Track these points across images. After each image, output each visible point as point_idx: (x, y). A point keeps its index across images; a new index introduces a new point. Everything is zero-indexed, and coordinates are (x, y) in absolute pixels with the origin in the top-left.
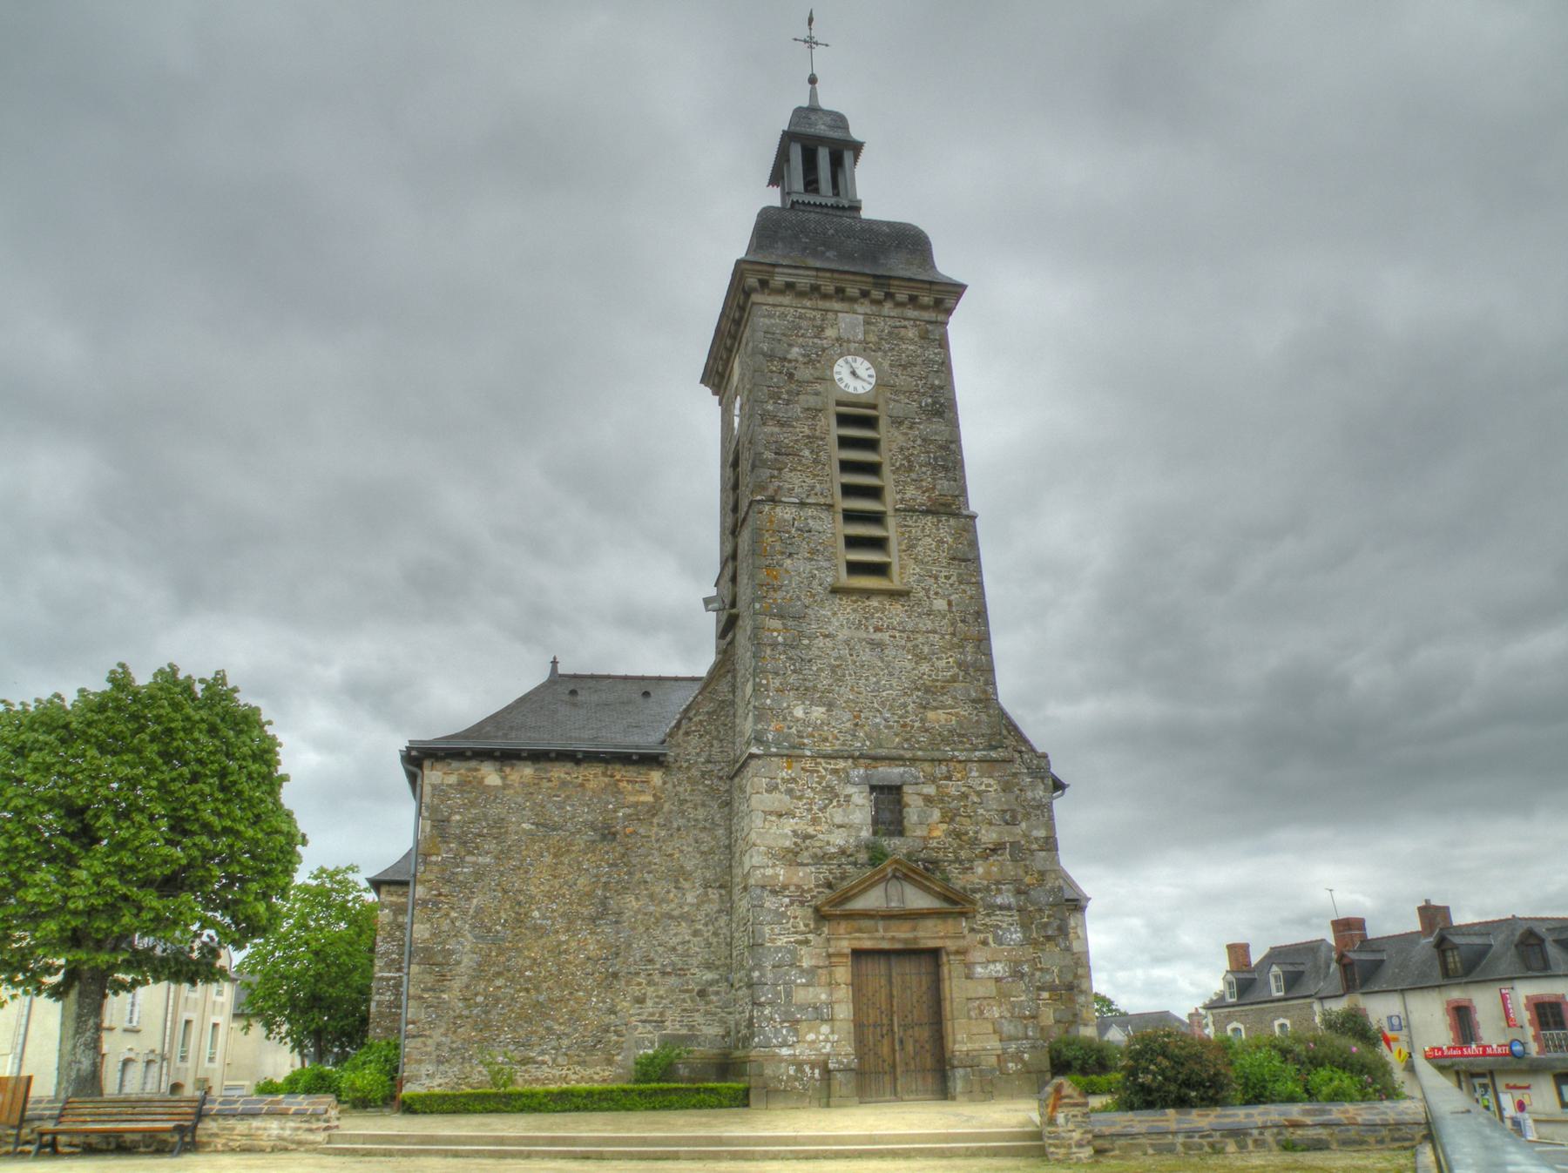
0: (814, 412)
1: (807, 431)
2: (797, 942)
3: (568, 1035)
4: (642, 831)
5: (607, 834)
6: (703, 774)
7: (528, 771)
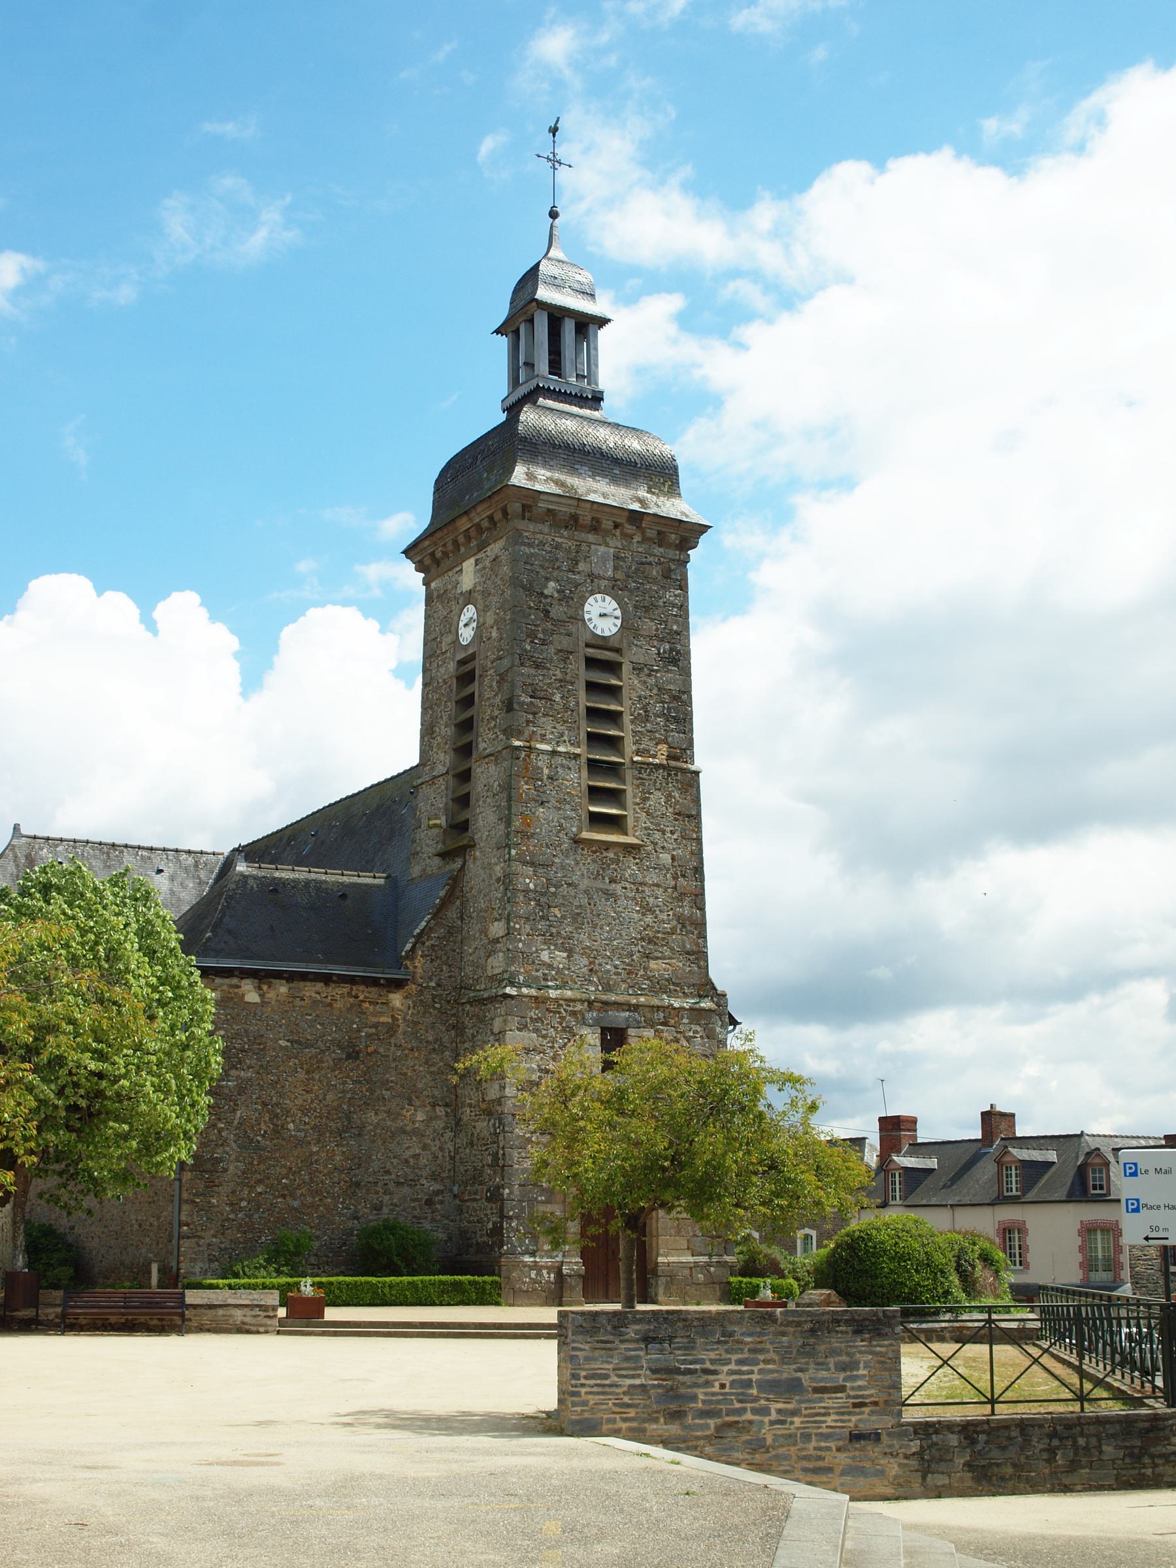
0: (565, 654)
1: (559, 676)
3: (318, 1238)
4: (381, 1050)
5: (353, 1054)
6: (434, 997)
7: (283, 989)
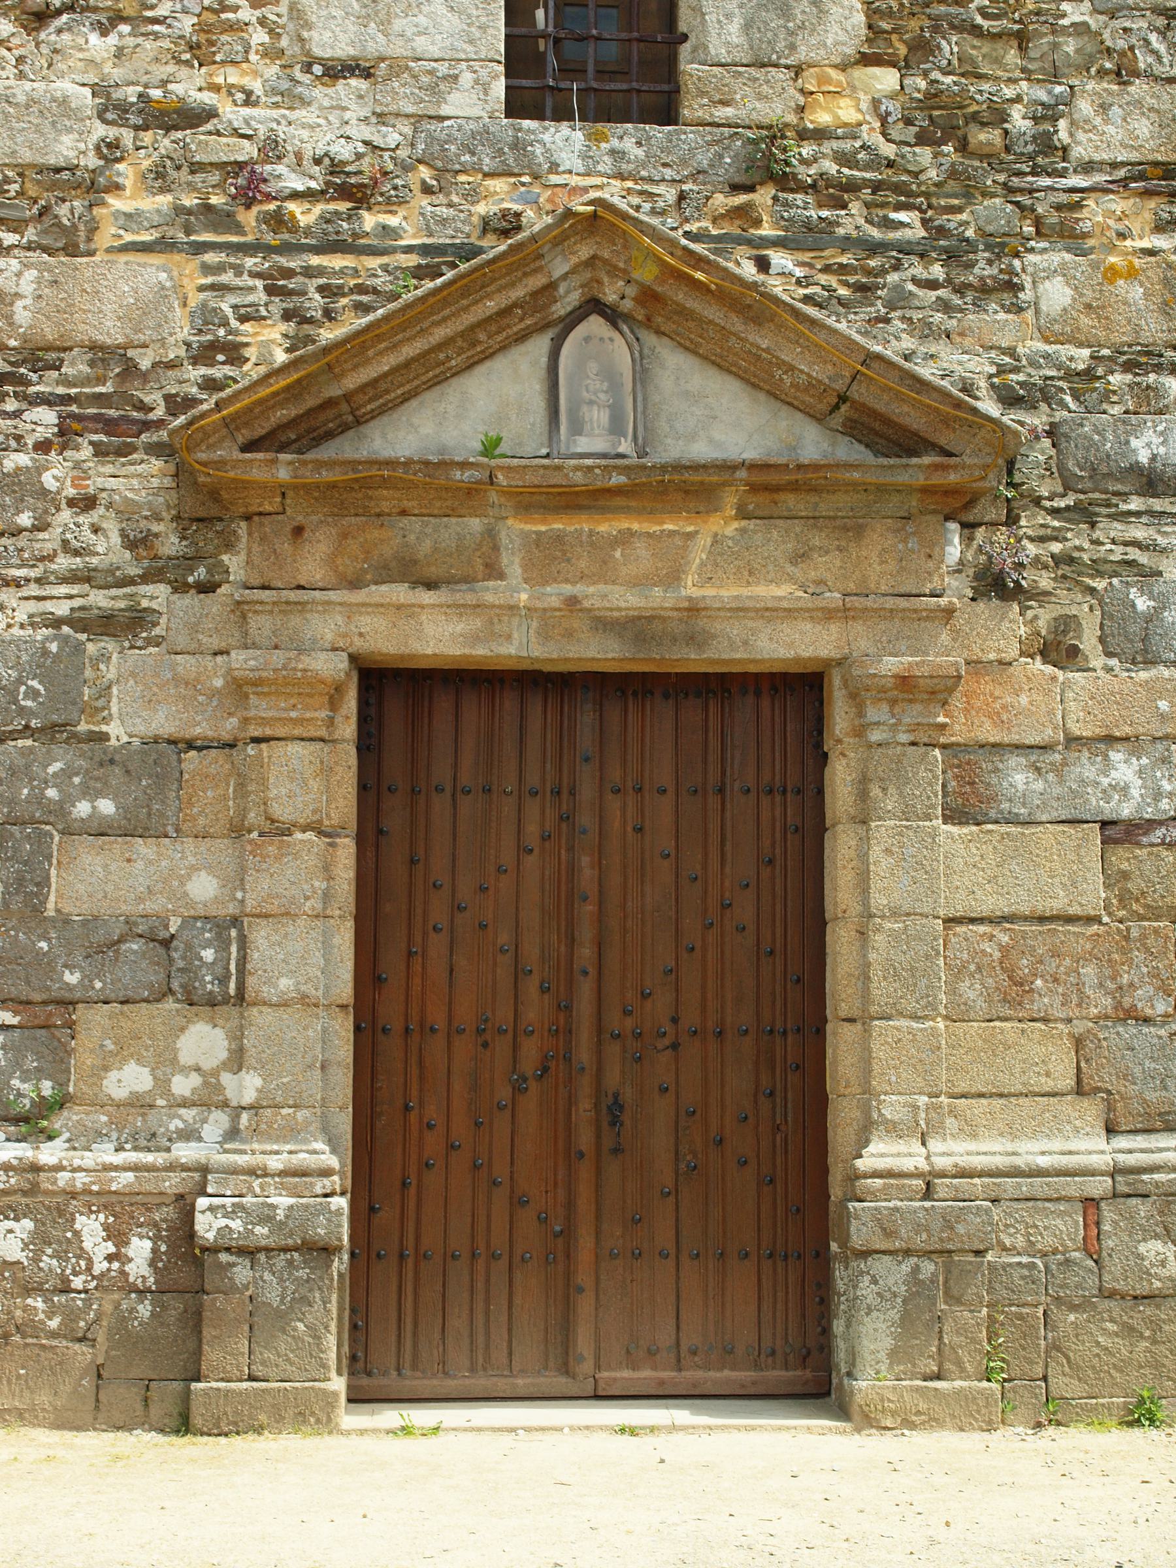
2: (84, 622)
